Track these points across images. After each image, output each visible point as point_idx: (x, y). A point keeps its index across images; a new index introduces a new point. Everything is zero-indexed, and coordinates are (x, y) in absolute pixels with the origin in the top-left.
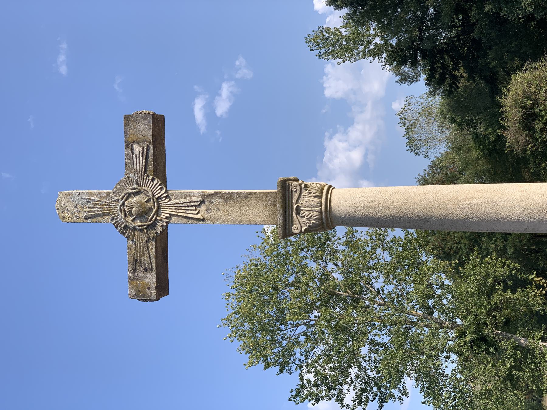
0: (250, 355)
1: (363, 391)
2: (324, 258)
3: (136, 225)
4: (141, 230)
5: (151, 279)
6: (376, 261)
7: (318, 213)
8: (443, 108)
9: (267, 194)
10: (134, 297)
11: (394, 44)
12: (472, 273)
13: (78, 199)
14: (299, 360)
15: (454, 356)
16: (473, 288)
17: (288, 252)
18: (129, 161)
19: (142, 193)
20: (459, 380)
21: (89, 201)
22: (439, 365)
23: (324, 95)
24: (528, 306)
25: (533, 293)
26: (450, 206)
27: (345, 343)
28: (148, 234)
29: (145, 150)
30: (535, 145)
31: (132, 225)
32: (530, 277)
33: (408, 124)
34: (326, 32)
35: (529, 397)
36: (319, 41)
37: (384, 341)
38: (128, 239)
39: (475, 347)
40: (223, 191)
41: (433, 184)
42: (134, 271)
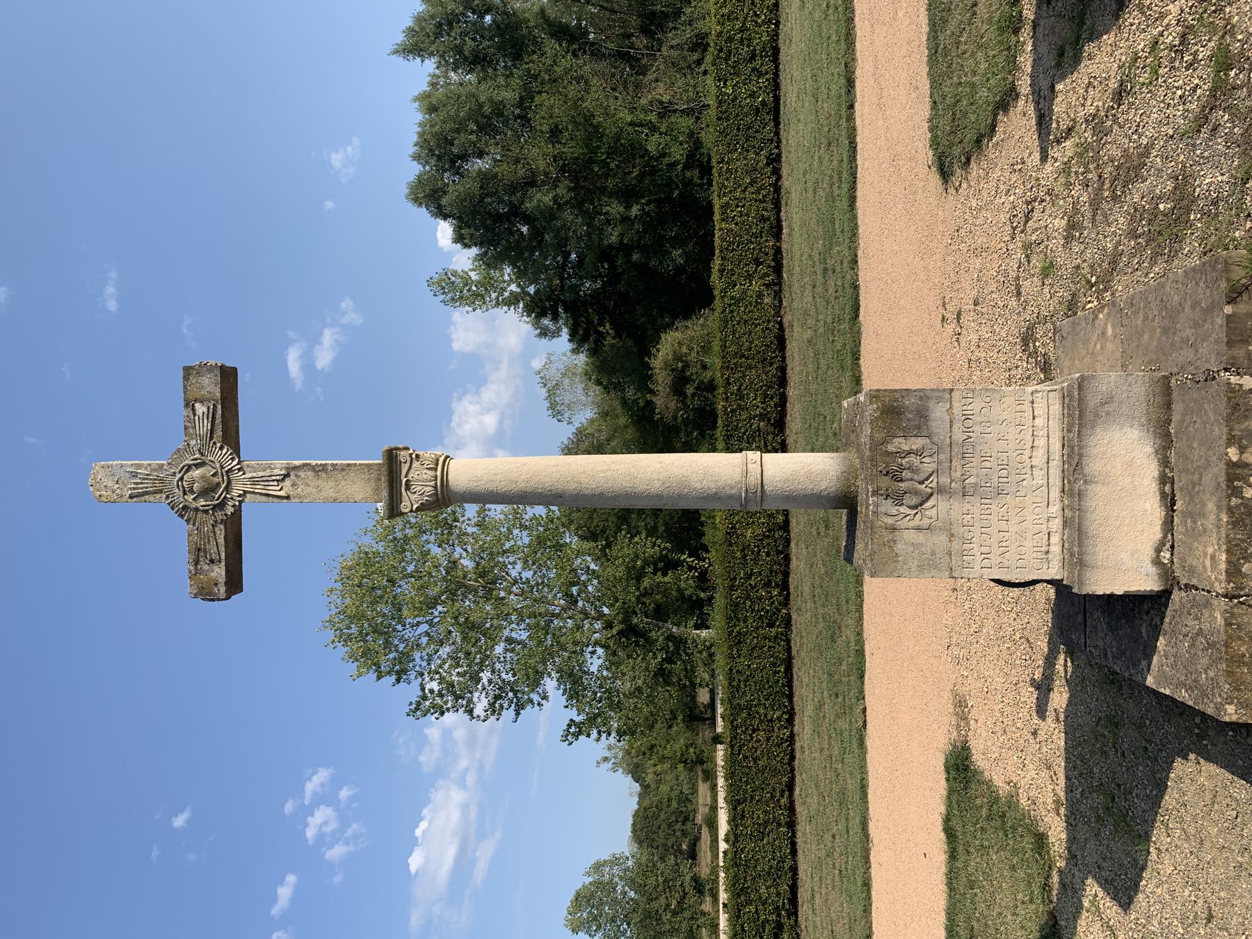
0: (358, 663)
1: (497, 698)
2: (451, 542)
3: (198, 505)
4: (206, 512)
5: (219, 572)
6: (512, 543)
7: (432, 488)
8: (588, 368)
9: (369, 466)
10: (196, 596)
11: (532, 292)
12: (620, 555)
13: (120, 473)
14: (420, 666)
15: (600, 651)
16: (621, 572)
17: (405, 536)
18: (189, 424)
19: (206, 464)
20: (605, 678)
21: (135, 475)
22: (583, 662)
23: (451, 348)
24: (680, 590)
25: (685, 576)
26: (584, 479)
27: (476, 642)
28: (215, 517)
29: (211, 411)
30: (686, 412)
31: (194, 505)
32: (682, 558)
33: (549, 385)
34: (452, 275)
35: (682, 693)
36: (444, 284)
37: (522, 637)
38: (188, 523)
39: (623, 639)
40: (314, 462)
41: (576, 454)
42: (197, 563)
